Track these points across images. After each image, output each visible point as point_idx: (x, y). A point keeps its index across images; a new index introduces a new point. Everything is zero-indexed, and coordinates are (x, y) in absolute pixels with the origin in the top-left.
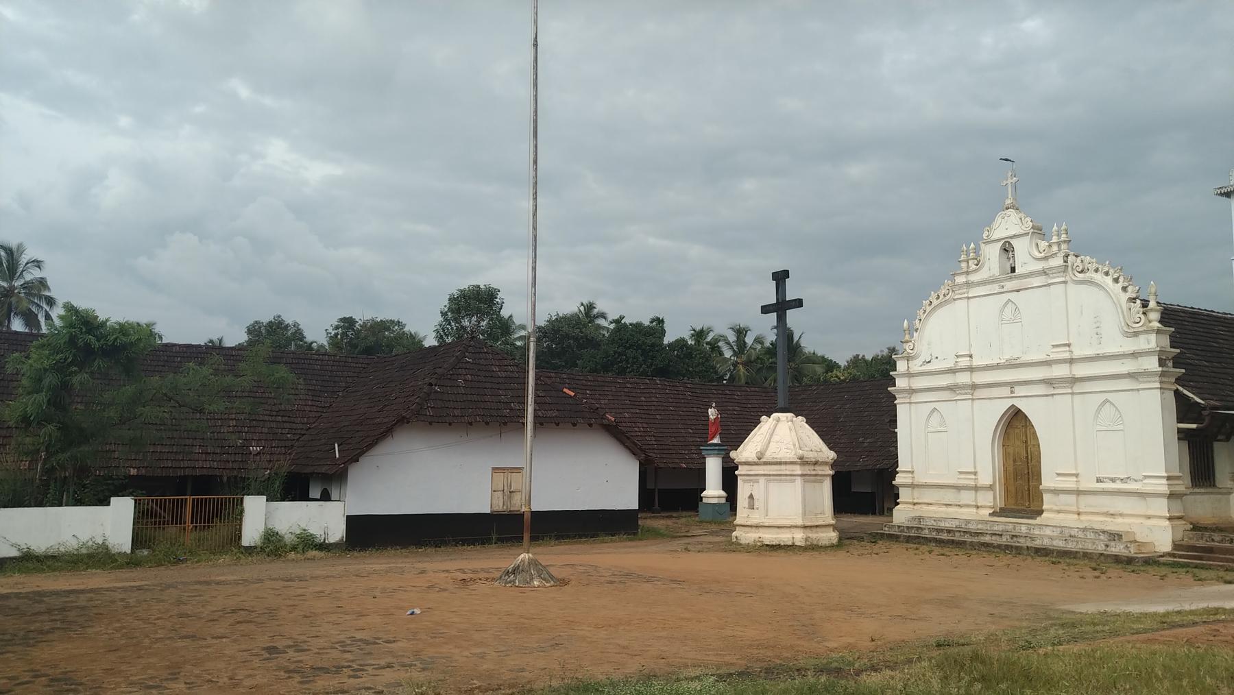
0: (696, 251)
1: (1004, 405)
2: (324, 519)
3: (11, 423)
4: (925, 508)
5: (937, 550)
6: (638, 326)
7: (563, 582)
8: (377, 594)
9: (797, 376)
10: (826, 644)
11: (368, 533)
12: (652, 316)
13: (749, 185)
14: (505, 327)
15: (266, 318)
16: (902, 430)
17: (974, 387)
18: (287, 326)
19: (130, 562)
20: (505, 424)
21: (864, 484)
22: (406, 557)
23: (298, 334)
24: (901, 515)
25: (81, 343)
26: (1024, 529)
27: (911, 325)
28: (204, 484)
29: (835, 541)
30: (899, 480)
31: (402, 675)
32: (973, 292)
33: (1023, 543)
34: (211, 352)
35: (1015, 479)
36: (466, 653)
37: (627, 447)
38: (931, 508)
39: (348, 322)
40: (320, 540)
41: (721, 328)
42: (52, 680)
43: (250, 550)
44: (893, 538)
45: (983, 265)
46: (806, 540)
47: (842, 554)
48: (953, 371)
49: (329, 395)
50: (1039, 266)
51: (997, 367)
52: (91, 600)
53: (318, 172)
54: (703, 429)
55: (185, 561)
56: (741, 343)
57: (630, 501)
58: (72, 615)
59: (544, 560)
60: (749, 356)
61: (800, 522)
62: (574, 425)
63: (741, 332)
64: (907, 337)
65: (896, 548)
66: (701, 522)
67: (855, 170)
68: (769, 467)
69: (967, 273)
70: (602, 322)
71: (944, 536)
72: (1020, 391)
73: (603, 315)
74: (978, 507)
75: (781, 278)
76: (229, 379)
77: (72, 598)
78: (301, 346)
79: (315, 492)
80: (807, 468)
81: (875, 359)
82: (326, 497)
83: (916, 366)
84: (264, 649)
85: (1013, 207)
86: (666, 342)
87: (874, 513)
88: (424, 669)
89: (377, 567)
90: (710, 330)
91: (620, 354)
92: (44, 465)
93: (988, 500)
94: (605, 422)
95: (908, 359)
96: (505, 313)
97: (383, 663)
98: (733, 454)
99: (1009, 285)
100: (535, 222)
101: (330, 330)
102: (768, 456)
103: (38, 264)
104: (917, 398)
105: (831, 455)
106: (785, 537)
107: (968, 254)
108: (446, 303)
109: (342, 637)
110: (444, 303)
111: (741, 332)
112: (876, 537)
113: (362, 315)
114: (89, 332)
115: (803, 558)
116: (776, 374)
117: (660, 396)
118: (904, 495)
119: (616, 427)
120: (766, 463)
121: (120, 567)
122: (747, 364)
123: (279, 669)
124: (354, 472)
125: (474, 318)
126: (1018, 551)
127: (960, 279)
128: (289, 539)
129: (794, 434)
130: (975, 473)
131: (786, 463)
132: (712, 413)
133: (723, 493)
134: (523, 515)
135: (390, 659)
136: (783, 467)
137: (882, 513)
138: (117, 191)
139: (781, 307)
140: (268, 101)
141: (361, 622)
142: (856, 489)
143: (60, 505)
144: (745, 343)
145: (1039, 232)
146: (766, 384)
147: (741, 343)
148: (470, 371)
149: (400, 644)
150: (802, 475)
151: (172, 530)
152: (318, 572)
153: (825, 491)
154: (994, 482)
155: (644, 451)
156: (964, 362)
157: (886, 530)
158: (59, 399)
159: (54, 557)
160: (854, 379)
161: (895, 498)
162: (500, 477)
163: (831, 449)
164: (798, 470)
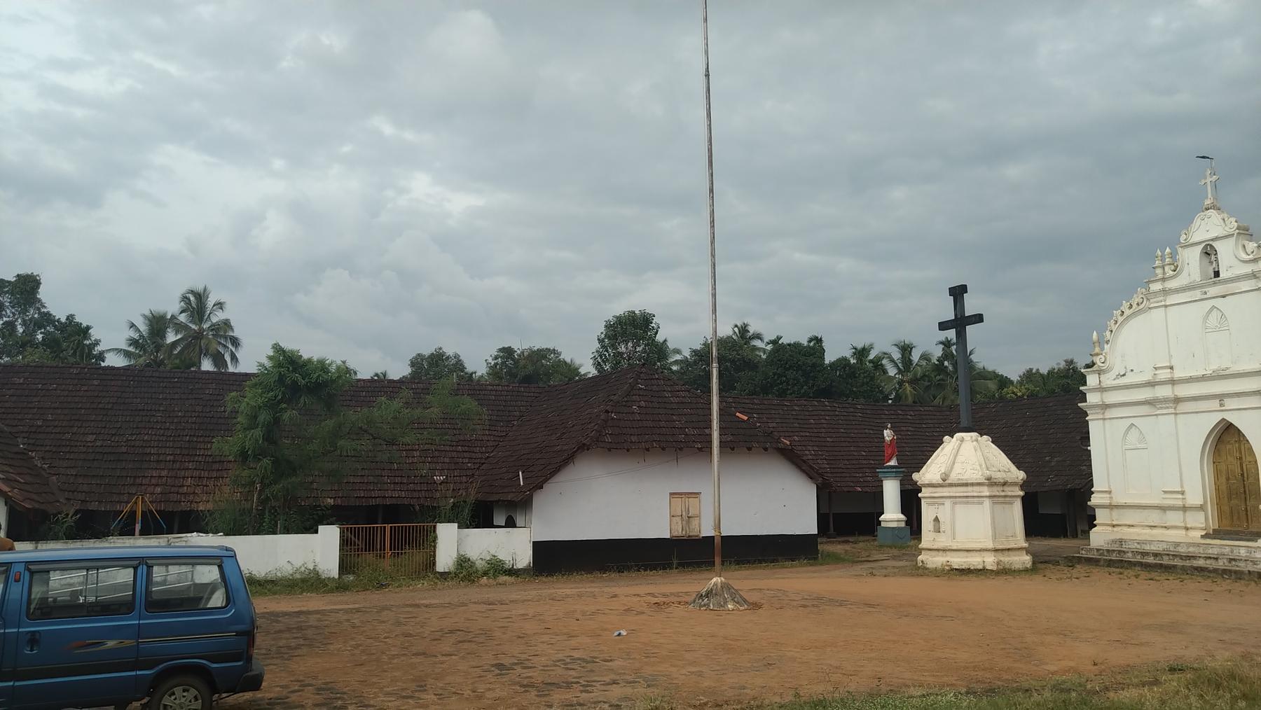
0: (845, 265)
1: (1215, 419)
2: (511, 545)
3: (231, 458)
4: (1126, 529)
5: (1144, 575)
6: (796, 346)
7: (756, 606)
8: (579, 617)
9: (973, 392)
10: (1047, 667)
11: (554, 559)
12: (810, 335)
13: (898, 193)
14: (661, 351)
15: (427, 352)
16: (1095, 447)
17: (1177, 400)
18: (448, 358)
19: (339, 587)
20: (681, 449)
21: (1057, 505)
22: (592, 582)
23: (459, 365)
24: (1099, 537)
25: (288, 381)
26: (1243, 552)
27: (1101, 336)
28: (393, 513)
29: (1029, 565)
30: (1095, 500)
31: (629, 691)
32: (1171, 300)
33: (1242, 566)
34: (380, 386)
35: (1230, 499)
36: (684, 671)
37: (804, 471)
38: (1132, 530)
39: (507, 352)
40: (508, 565)
41: (883, 344)
42: (319, 689)
43: (444, 576)
44: (1089, 561)
45: (1182, 270)
46: (998, 564)
47: (1038, 578)
48: (1151, 384)
49: (496, 429)
50: (1248, 269)
51: (1203, 378)
52: (319, 620)
53: (461, 203)
54: (878, 452)
55: (387, 586)
56: (906, 361)
57: (806, 523)
58: (309, 633)
59: (736, 585)
60: (915, 374)
61: (990, 545)
62: (749, 449)
63: (906, 349)
64: (1097, 350)
65: (1098, 573)
66: (881, 546)
67: (1013, 172)
68: (954, 489)
69: (1164, 280)
70: (757, 343)
71: (1151, 560)
72: (1231, 404)
73: (758, 336)
74: (1187, 529)
75: (958, 293)
76: (418, 412)
77: (303, 618)
78: (463, 377)
79: (500, 519)
80: (995, 488)
81: (1051, 373)
82: (511, 524)
83: (1108, 380)
84: (493, 666)
85: (1214, 207)
86: (827, 362)
87: (1065, 536)
88: (649, 686)
89: (568, 591)
90: (871, 347)
91: (780, 376)
92: (260, 495)
93: (1200, 522)
94: (780, 446)
95: (1100, 372)
96: (660, 338)
97: (607, 679)
98: (915, 476)
99: (1213, 291)
100: (713, 250)
101: (490, 360)
102: (953, 478)
103: (220, 305)
104: (1110, 413)
105: (1021, 475)
106: (975, 561)
107: (1163, 259)
108: (603, 329)
109: (560, 656)
110: (600, 329)
111: (906, 349)
112: (1073, 561)
113: (520, 345)
114: (295, 370)
115: (999, 582)
116: (942, 394)
117: (841, 421)
118: (1101, 517)
119: (792, 450)
120: (951, 485)
121: (331, 591)
122: (913, 382)
123: (515, 684)
124: (539, 499)
125: (630, 344)
126: (1238, 575)
127: (1156, 287)
128: (480, 565)
129: (979, 453)
130: (1183, 493)
131: (972, 484)
132: (888, 434)
133: (902, 517)
134: (713, 537)
135: (613, 677)
136: (970, 488)
137: (1075, 536)
138: (275, 230)
139: (961, 322)
140: (409, 136)
141: (573, 642)
142: (1042, 511)
143: (275, 533)
144: (910, 361)
145: (1245, 232)
146: (936, 402)
147: (906, 361)
148: (640, 397)
149: (616, 663)
150: (990, 497)
151: (370, 557)
152: (514, 596)
153: (1015, 514)
154: (1205, 502)
155: (821, 475)
156: (1164, 375)
157: (1084, 554)
158: (272, 432)
159: (272, 581)
160: (1032, 395)
161: (1091, 521)
162: (677, 502)
163: (1019, 468)
164: (986, 491)
